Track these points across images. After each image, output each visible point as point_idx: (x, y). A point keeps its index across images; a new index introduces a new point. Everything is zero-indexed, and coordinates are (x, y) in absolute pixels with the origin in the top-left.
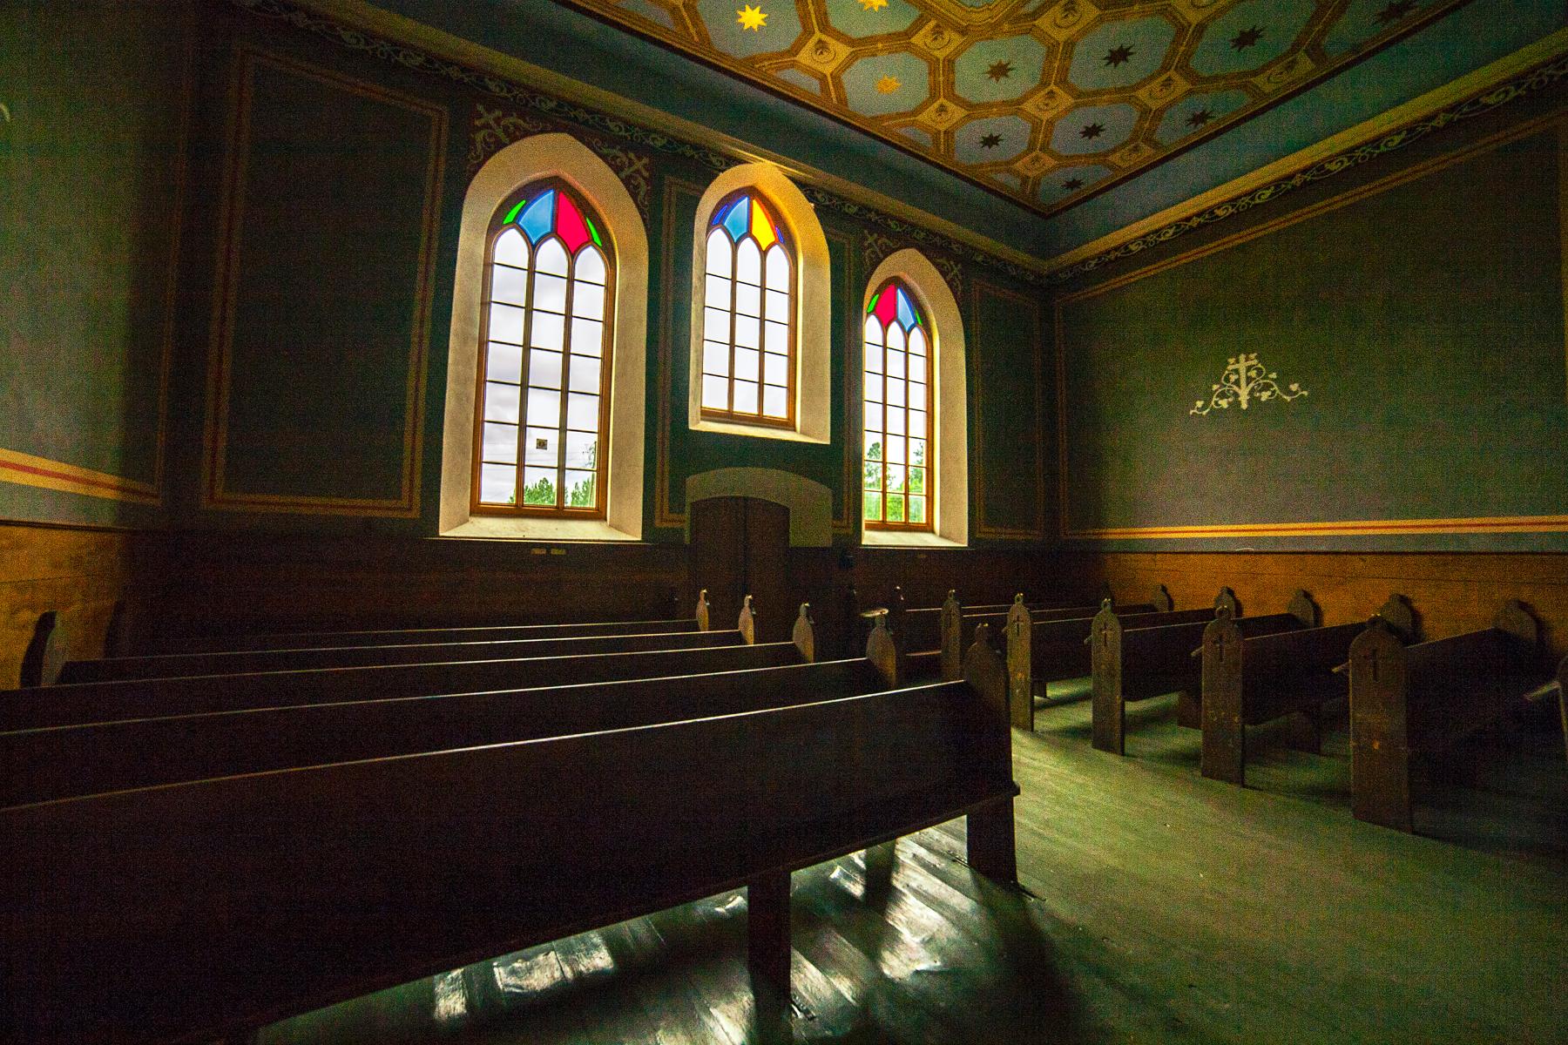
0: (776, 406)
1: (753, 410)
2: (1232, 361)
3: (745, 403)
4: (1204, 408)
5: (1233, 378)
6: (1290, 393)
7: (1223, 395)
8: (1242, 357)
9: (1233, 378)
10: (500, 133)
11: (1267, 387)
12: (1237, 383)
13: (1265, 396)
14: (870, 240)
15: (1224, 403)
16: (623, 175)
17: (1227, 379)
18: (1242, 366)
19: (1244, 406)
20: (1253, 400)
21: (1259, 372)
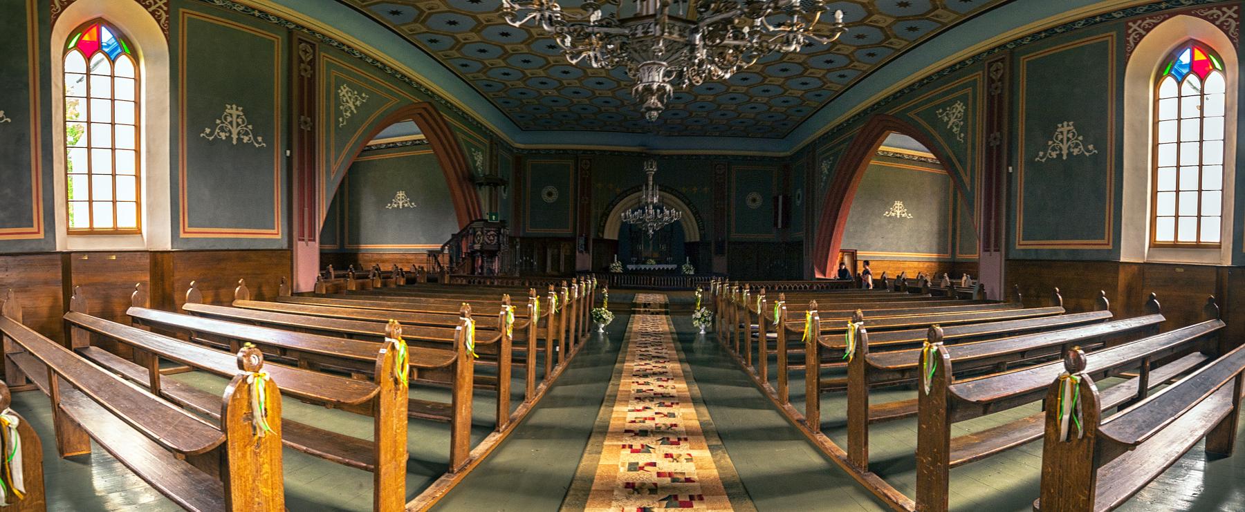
0: (127, 220)
1: (110, 225)
3: (103, 221)
4: (209, 135)
5: (1060, 137)
6: (1088, 151)
9: (1060, 137)
10: (1141, 31)
11: (1077, 145)
12: (1062, 141)
14: (1230, 12)
16: (446, 400)
18: (1065, 130)
19: (235, 142)
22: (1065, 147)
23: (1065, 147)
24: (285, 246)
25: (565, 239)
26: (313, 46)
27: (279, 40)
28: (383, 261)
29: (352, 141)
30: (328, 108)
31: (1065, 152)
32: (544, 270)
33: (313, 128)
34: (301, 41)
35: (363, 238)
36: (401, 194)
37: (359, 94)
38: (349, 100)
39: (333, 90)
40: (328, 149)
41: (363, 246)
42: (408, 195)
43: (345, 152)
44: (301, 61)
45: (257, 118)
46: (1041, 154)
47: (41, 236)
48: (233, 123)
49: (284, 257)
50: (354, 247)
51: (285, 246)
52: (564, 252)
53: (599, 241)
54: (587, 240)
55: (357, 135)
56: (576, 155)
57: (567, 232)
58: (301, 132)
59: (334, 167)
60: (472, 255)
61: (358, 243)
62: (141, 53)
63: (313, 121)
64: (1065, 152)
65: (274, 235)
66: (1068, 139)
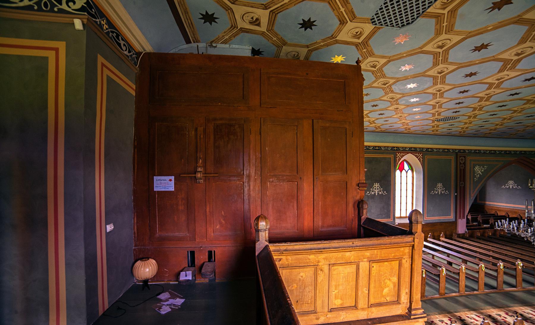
7: (373, 191)
11: (380, 191)
15: (373, 193)
18: (377, 185)
20: (441, 193)
24: (454, 220)
26: (465, 157)
27: (453, 158)
28: (500, 211)
29: (480, 185)
30: (470, 176)
33: (465, 185)
34: (460, 156)
35: (488, 197)
36: (511, 182)
37: (483, 167)
38: (479, 170)
39: (472, 169)
40: (470, 190)
41: (487, 203)
42: (515, 182)
43: (477, 189)
44: (461, 163)
45: (446, 187)
47: (62, 46)
48: (439, 188)
49: (454, 224)
50: (483, 202)
51: (454, 220)
55: (482, 182)
58: (460, 187)
59: (472, 195)
61: (485, 201)
62: (414, 170)
63: (465, 183)
65: (451, 217)
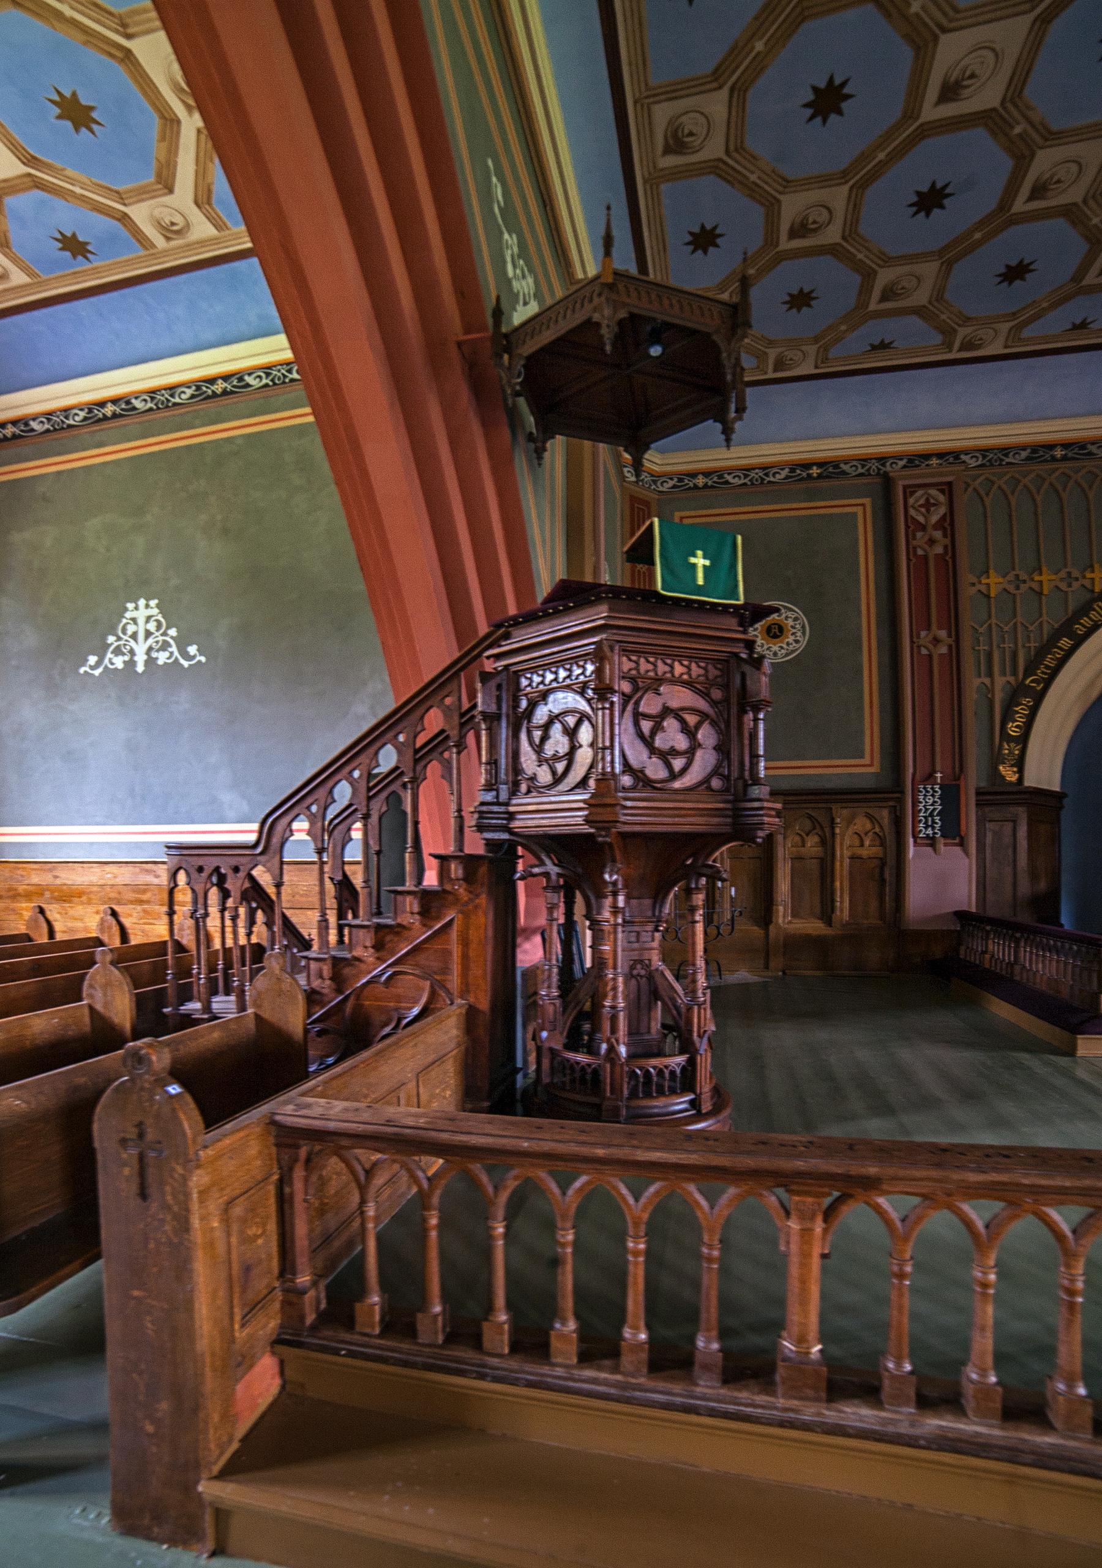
2: (131, 606)
5: (131, 629)
6: (190, 658)
7: (118, 651)
8: (142, 602)
9: (131, 629)
11: (165, 646)
12: (134, 636)
13: (162, 658)
17: (124, 631)
18: (141, 614)
19: (140, 668)
20: (150, 662)
21: (159, 625)
22: (141, 650)
23: (141, 650)
25: (851, 795)
28: (67, 896)
31: (140, 659)
32: (764, 913)
46: (93, 660)
52: (855, 837)
53: (999, 797)
54: (951, 796)
56: (881, 479)
57: (864, 766)
60: (493, 869)
64: (140, 659)
66: (148, 634)
